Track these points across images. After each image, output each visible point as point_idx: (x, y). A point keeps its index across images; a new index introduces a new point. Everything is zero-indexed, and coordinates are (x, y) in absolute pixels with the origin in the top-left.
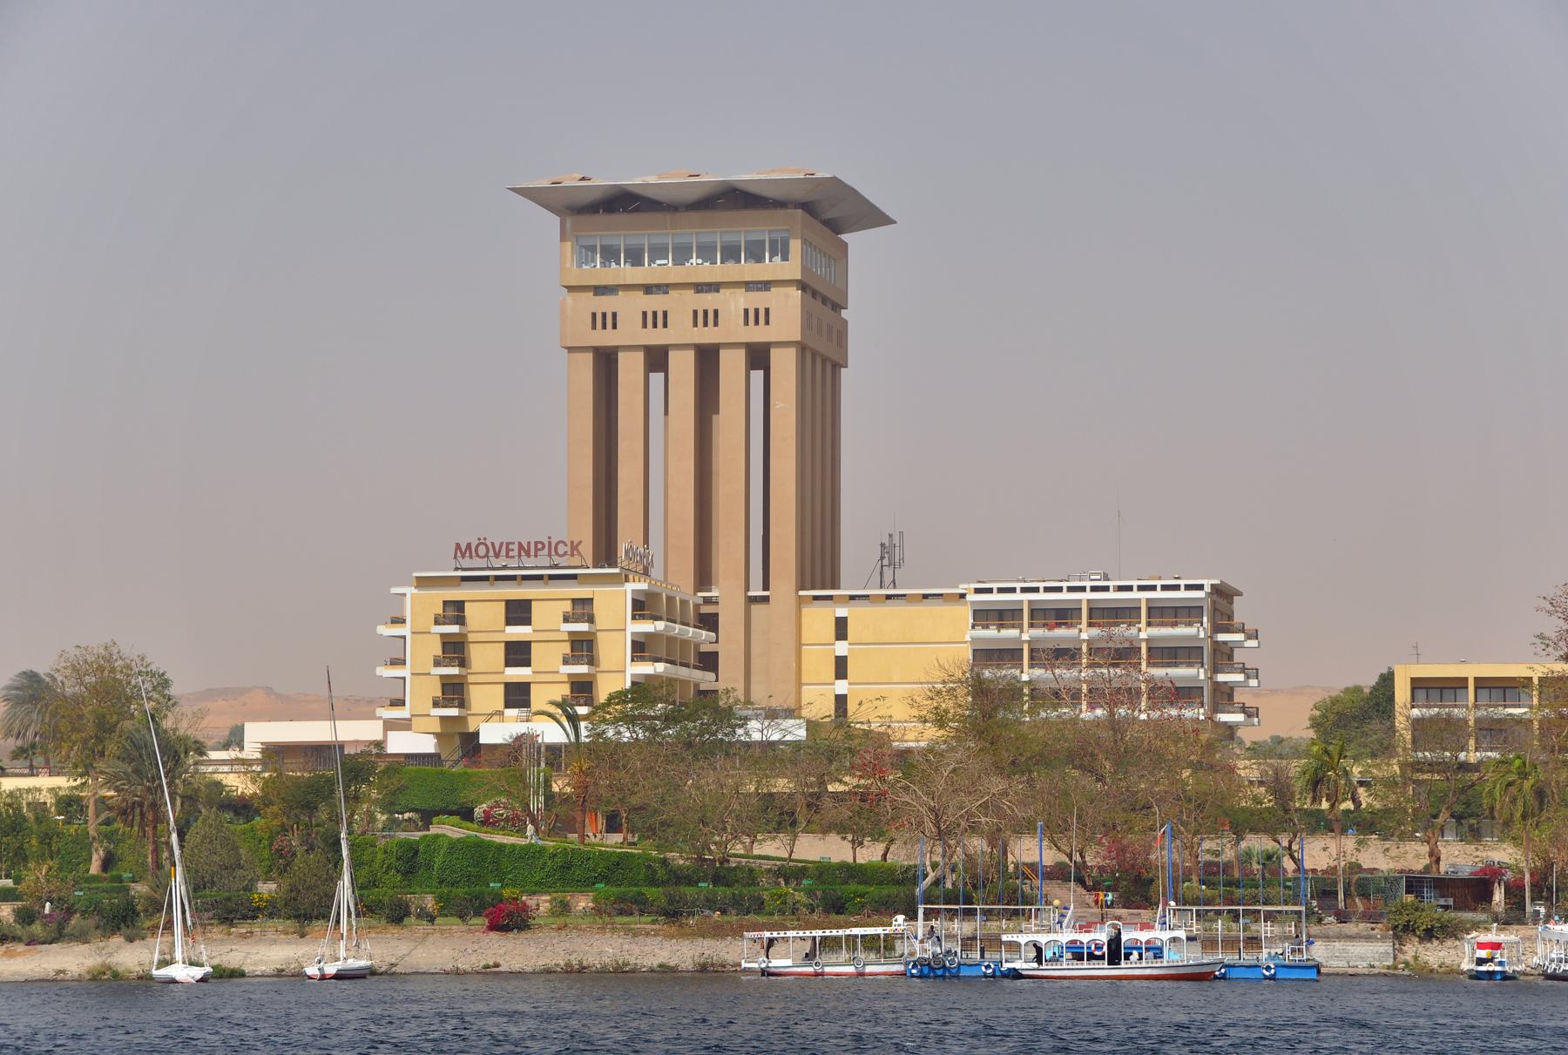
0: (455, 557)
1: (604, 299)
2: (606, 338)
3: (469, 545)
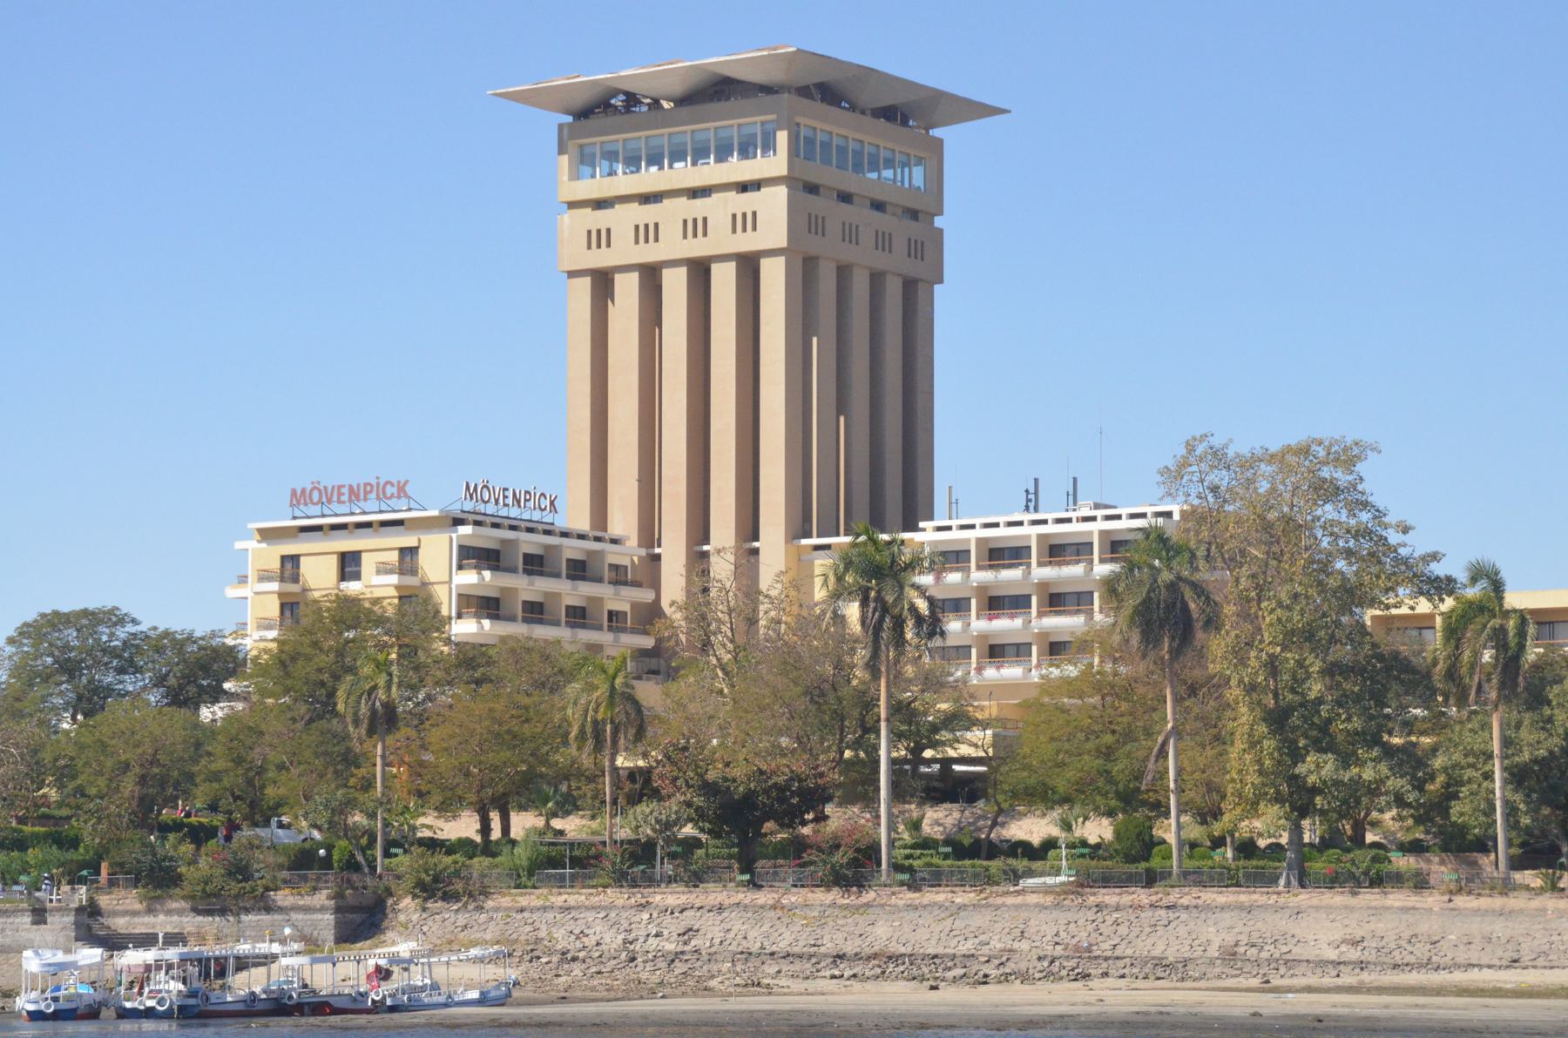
0: (291, 505)
1: (699, 202)
2: (601, 259)
3: (303, 491)
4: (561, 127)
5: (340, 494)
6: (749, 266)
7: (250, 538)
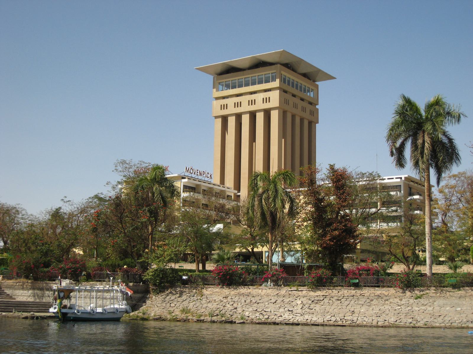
1: (253, 95)
2: (225, 112)
6: (267, 113)
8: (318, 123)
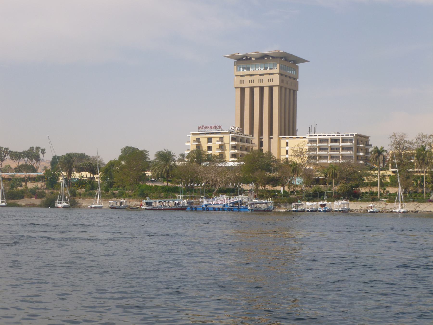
0: (198, 129)
1: (262, 76)
2: (242, 85)
4: (235, 62)
5: (208, 128)
6: (271, 89)
7: (190, 135)
8: (298, 91)
